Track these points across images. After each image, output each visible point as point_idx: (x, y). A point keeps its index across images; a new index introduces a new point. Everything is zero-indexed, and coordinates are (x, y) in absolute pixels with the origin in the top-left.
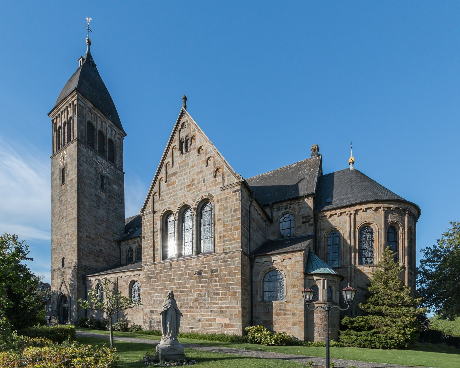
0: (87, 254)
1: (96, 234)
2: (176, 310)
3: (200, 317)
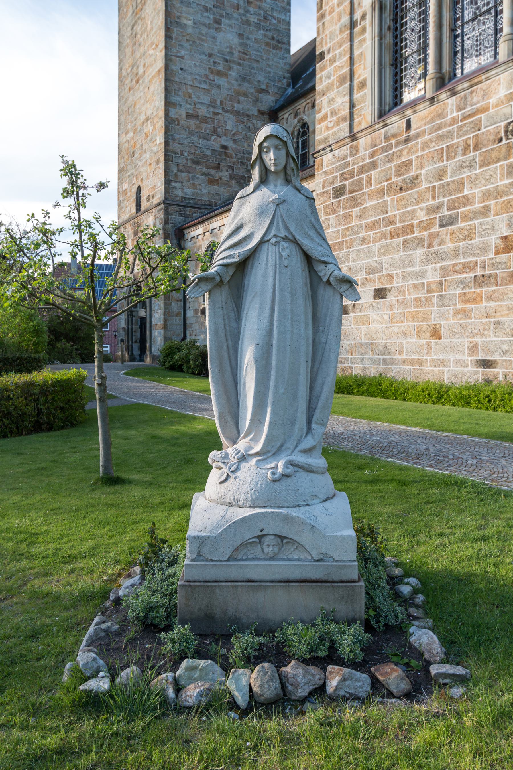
0: (189, 163)
1: (212, 104)
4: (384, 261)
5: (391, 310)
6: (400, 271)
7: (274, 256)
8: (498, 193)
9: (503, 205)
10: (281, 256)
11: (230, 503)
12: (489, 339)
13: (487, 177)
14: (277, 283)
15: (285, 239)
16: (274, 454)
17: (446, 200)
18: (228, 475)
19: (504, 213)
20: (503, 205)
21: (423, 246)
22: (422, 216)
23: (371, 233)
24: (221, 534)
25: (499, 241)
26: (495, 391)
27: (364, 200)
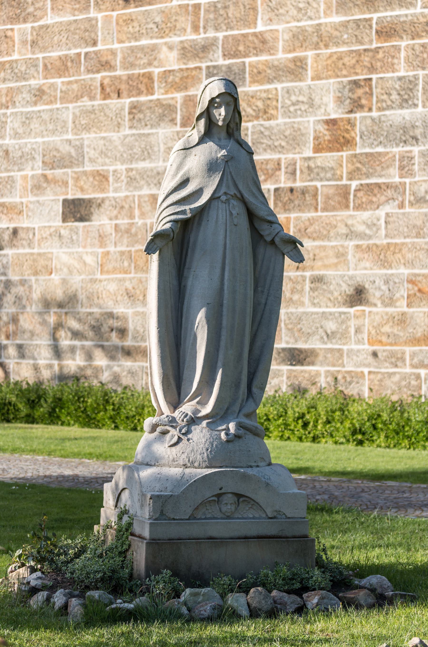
2: (251, 215)
3: (363, 271)
4: (86, 143)
5: (102, 244)
6: (124, 167)
7: (224, 213)
8: (320, 37)
9: (329, 62)
10: (231, 214)
11: (184, 465)
12: (301, 310)
13: (301, 5)
14: (228, 242)
15: (234, 196)
16: (221, 417)
17: (220, 35)
18: (179, 438)
19: (330, 77)
20: (329, 62)
21: (173, 121)
22: (171, 60)
23: (59, 81)
24: (183, 492)
25: (322, 128)
26: (314, 407)
27: (43, 9)
